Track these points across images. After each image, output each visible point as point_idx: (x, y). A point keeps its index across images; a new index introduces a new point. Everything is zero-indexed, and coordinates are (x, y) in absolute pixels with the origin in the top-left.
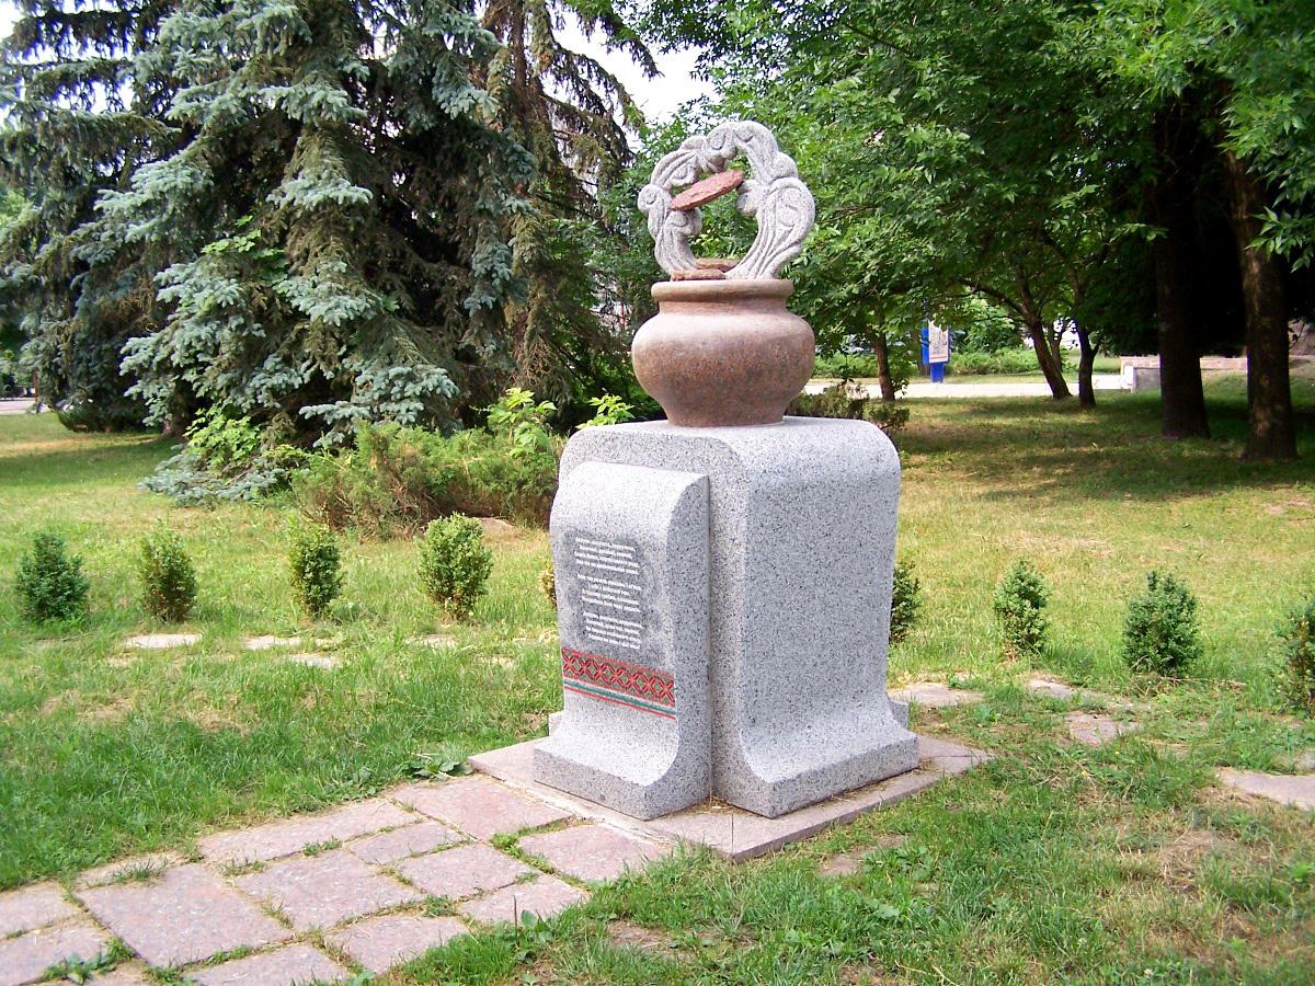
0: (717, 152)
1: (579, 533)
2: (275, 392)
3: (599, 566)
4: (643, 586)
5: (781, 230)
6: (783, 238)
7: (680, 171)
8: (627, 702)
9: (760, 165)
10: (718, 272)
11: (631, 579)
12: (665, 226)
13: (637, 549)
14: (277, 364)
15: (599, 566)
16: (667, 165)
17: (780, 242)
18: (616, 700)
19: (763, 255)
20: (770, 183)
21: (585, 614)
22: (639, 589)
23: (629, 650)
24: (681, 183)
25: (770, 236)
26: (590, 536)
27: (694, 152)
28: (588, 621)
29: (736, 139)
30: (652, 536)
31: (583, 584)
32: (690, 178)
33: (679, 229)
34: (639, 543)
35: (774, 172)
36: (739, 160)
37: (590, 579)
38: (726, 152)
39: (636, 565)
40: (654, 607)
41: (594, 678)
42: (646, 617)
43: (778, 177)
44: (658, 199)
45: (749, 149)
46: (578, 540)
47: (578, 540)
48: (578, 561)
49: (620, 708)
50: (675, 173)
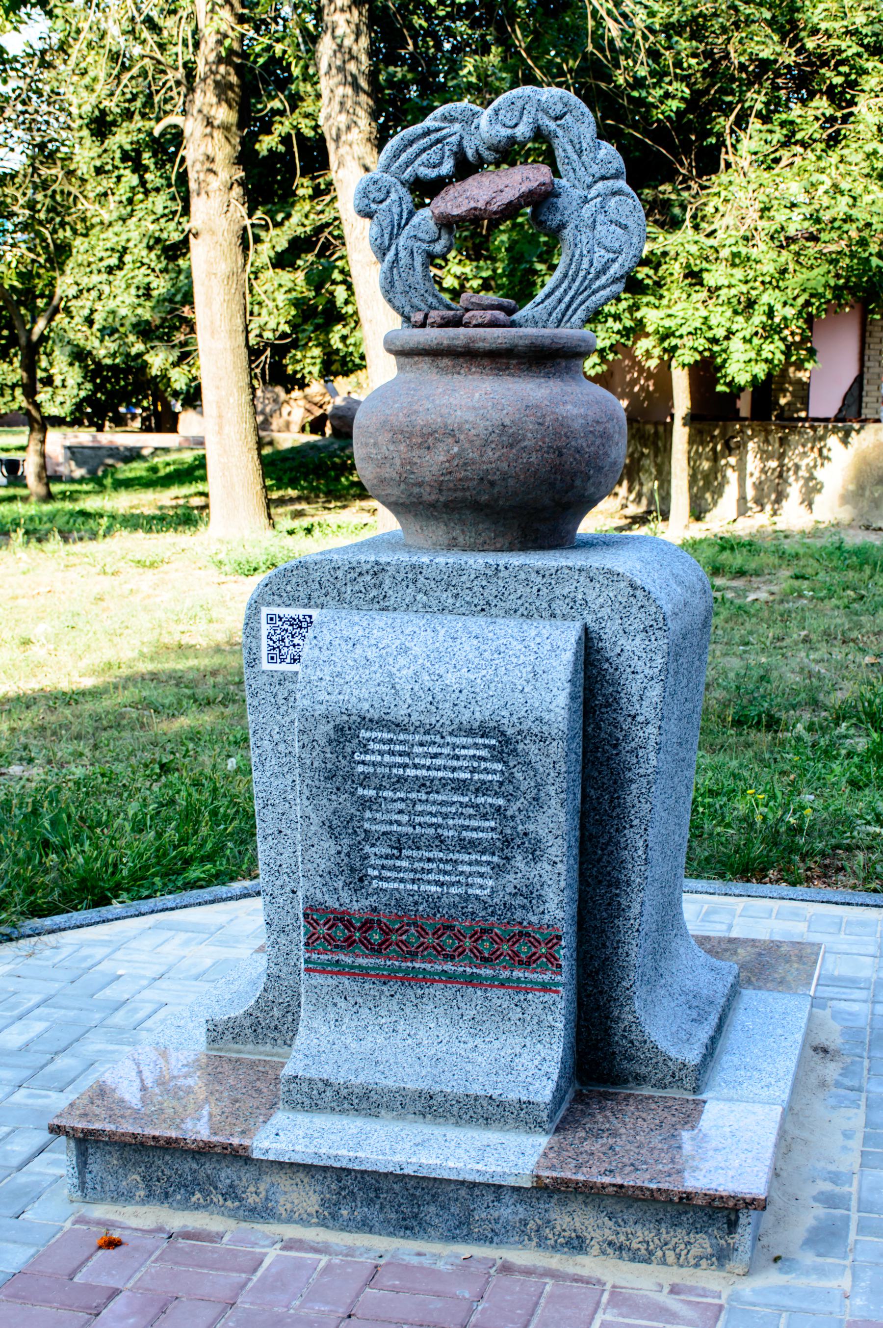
0: (509, 132)
1: (366, 722)
2: (74, 452)
3: (411, 772)
4: (510, 798)
5: (601, 256)
6: (604, 270)
7: (432, 155)
8: (450, 979)
9: (575, 157)
10: (501, 315)
11: (482, 789)
12: (402, 240)
13: (504, 743)
14: (827, 285)
15: (411, 772)
16: (411, 143)
17: (597, 277)
18: (428, 979)
19: (571, 293)
20: (589, 187)
21: (367, 849)
22: (501, 802)
23: (466, 898)
24: (432, 173)
25: (585, 265)
26: (399, 726)
27: (457, 127)
28: (372, 861)
29: (540, 115)
30: (540, 719)
31: (365, 804)
32: (447, 167)
33: (425, 246)
34: (510, 732)
35: (595, 169)
36: (541, 147)
37: (388, 794)
38: (523, 131)
39: (499, 766)
40: (531, 827)
41: (376, 950)
42: (510, 844)
43: (603, 178)
44: (393, 196)
45: (560, 133)
46: (364, 734)
47: (364, 734)
48: (360, 768)
49: (436, 990)
50: (424, 156)
